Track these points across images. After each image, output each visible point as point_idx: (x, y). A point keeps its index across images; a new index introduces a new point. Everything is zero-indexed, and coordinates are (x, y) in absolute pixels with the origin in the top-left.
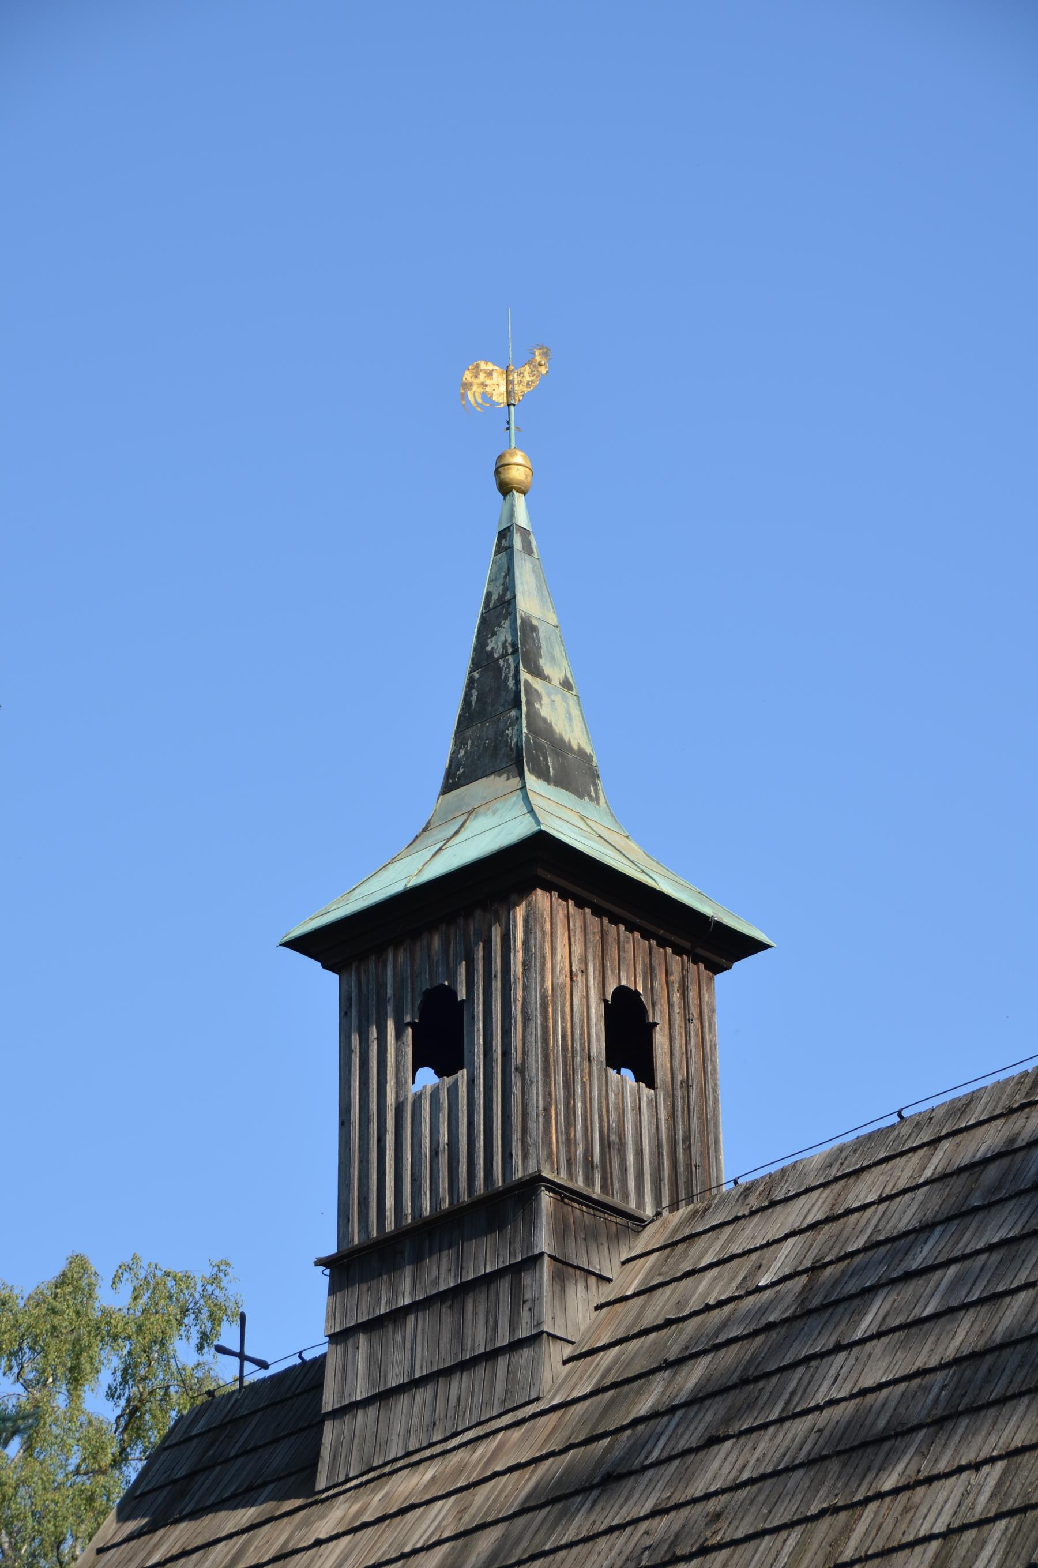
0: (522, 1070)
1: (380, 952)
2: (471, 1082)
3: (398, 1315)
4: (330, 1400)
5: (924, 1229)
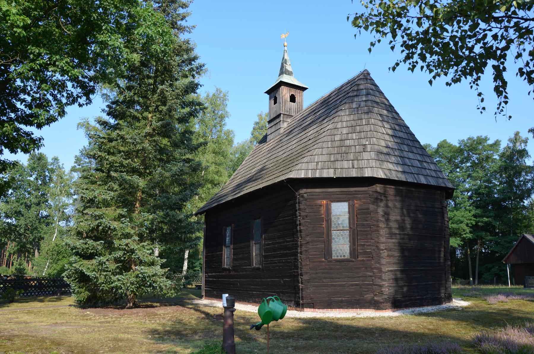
3: (272, 126)
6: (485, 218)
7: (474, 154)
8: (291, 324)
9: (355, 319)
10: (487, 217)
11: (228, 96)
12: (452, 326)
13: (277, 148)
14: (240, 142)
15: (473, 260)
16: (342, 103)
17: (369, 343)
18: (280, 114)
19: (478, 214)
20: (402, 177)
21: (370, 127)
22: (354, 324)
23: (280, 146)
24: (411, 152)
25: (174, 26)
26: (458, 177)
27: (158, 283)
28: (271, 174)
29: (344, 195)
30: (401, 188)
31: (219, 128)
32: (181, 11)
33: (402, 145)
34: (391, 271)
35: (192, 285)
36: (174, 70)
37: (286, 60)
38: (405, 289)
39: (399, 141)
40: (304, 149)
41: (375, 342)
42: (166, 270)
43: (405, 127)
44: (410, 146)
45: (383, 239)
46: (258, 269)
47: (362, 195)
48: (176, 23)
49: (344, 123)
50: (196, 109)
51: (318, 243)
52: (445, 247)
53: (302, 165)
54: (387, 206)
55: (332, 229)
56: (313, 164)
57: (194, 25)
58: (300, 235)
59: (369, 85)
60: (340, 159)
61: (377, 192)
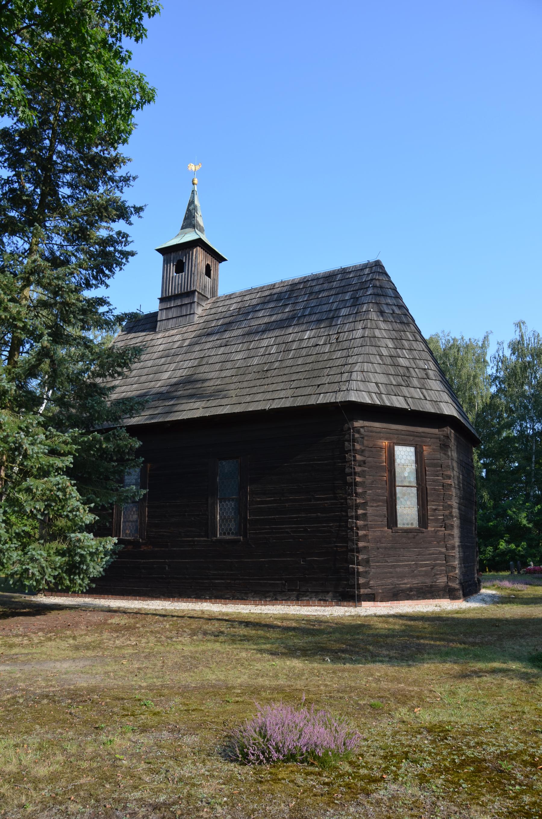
0: (194, 274)
1: (171, 253)
2: (185, 274)
3: (171, 308)
4: (159, 319)
5: (258, 304)
29: (411, 436)
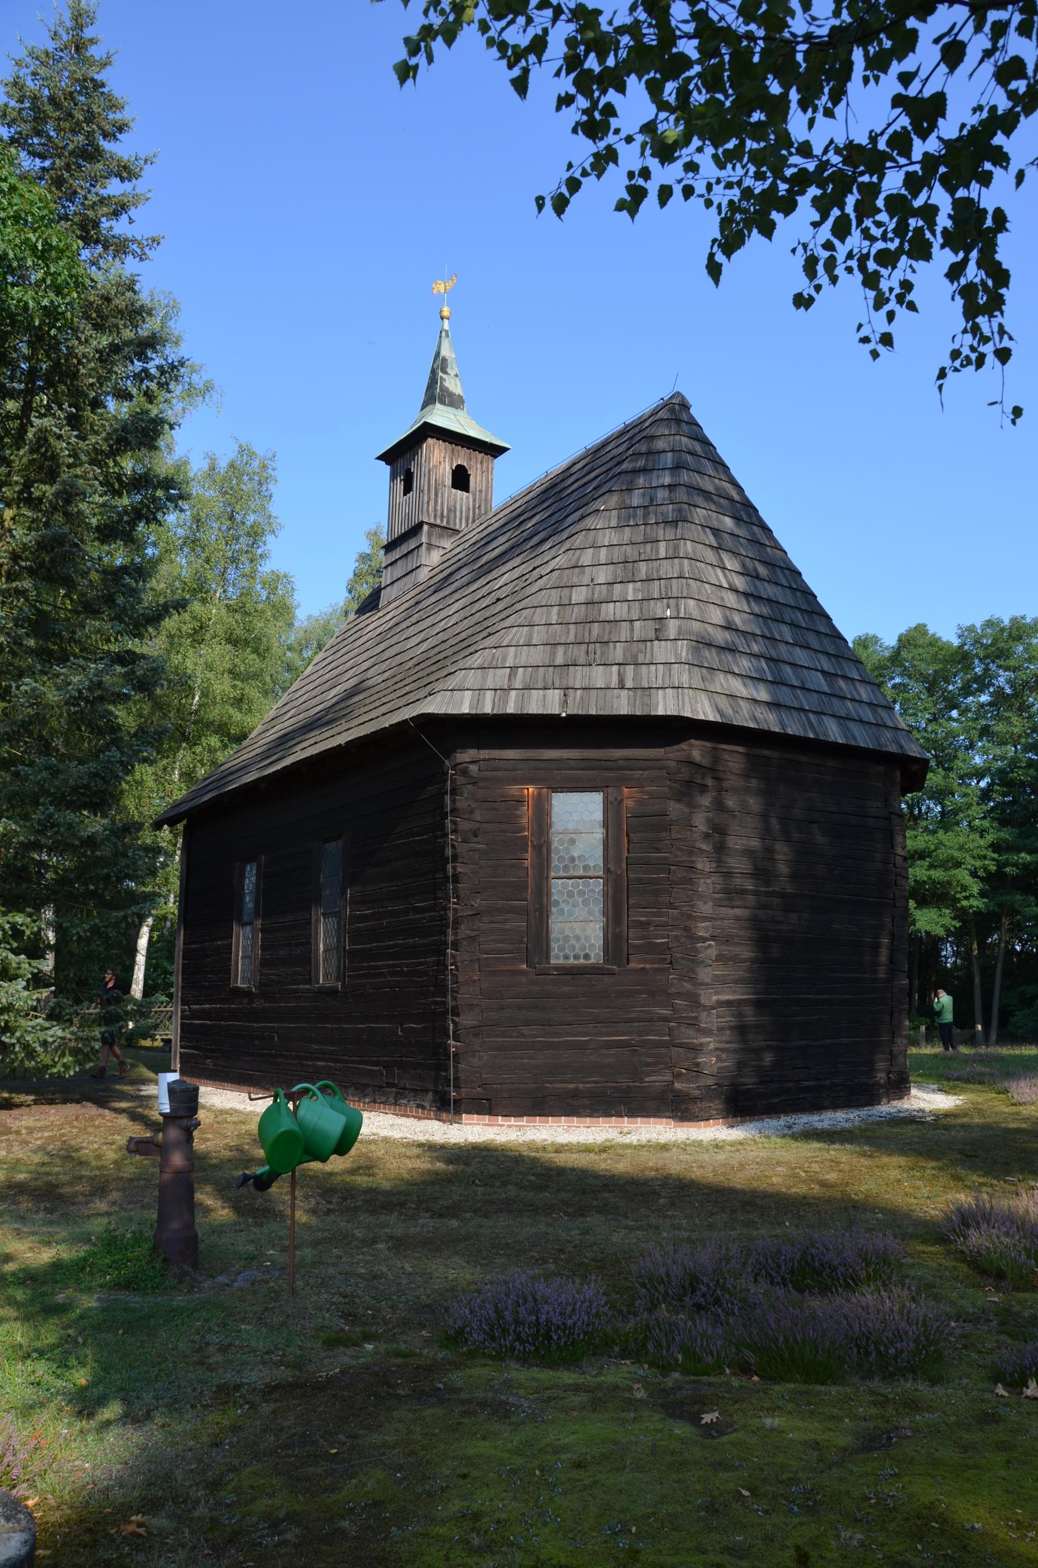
3: (396, 561)
6: (1023, 855)
7: (1000, 667)
8: (410, 1164)
9: (610, 1148)
10: (1030, 852)
11: (274, 470)
12: (894, 1174)
13: (403, 625)
14: (316, 614)
15: (987, 973)
16: (600, 492)
17: (631, 1229)
18: (421, 524)
19: (1006, 841)
20: (770, 721)
21: (681, 565)
22: (603, 1166)
23: (413, 620)
24: (801, 646)
25: (88, 232)
26: (952, 734)
27: (18, 1034)
28: (377, 704)
29: (593, 769)
30: (766, 752)
31: (247, 568)
32: (114, 188)
33: (775, 624)
34: (728, 1003)
35: (154, 1040)
36: (83, 371)
37: (444, 360)
38: (768, 1058)
39: (765, 610)
40: (478, 628)
41: (650, 1226)
42: (45, 995)
43: (787, 572)
44: (799, 627)
45: (706, 908)
46: (332, 992)
47: (647, 772)
48: (96, 224)
49: (603, 550)
50: (154, 499)
51: (507, 916)
52: (893, 935)
53: (465, 677)
54: (719, 806)
55: (553, 874)
56: (499, 672)
57: (155, 234)
58: (455, 890)
59: (685, 440)
60: (582, 660)
61: (691, 763)
